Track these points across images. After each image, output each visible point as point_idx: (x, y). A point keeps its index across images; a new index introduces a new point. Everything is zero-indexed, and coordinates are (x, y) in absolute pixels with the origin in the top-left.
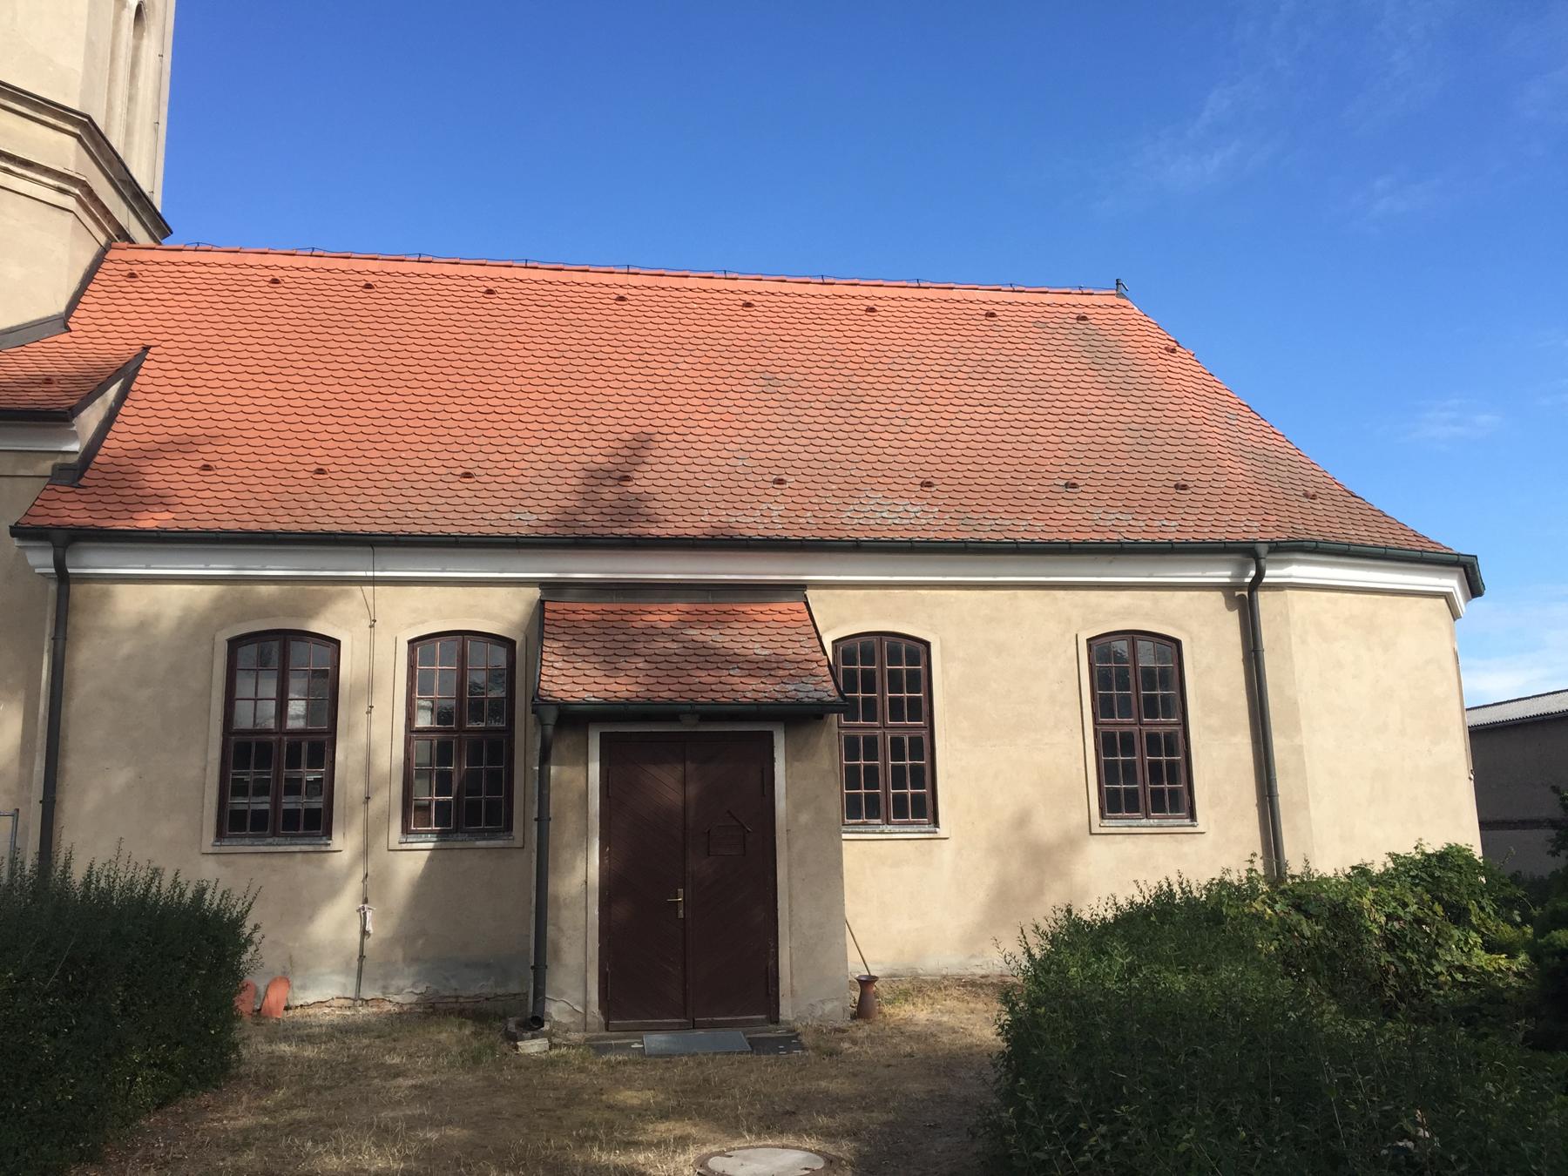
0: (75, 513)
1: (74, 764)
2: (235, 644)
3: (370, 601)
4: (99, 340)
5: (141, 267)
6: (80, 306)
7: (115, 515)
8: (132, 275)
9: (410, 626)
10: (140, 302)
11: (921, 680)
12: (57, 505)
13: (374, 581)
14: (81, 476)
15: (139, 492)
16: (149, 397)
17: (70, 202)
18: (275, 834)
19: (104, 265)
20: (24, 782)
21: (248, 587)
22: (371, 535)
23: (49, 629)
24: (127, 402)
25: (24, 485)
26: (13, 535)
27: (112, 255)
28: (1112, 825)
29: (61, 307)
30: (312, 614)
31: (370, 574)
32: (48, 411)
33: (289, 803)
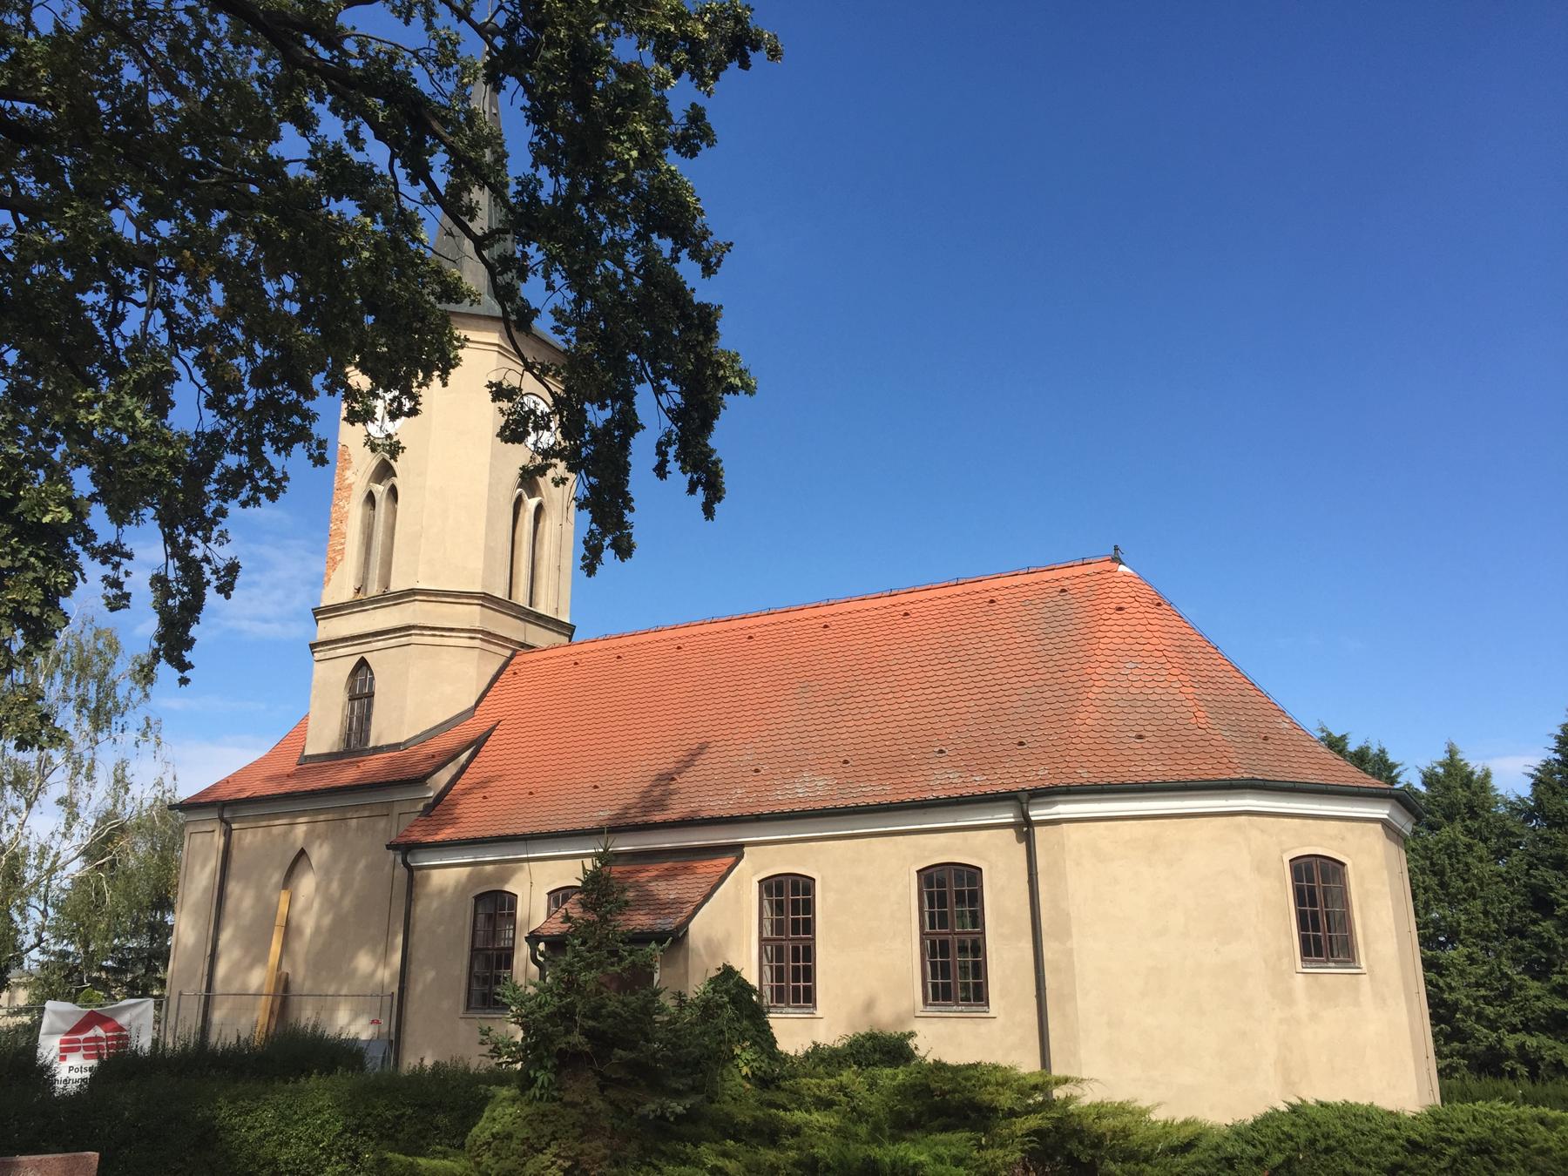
2: (478, 898)
11: (975, 898)
13: (528, 860)
17: (477, 643)
28: (931, 1011)
30: (505, 880)
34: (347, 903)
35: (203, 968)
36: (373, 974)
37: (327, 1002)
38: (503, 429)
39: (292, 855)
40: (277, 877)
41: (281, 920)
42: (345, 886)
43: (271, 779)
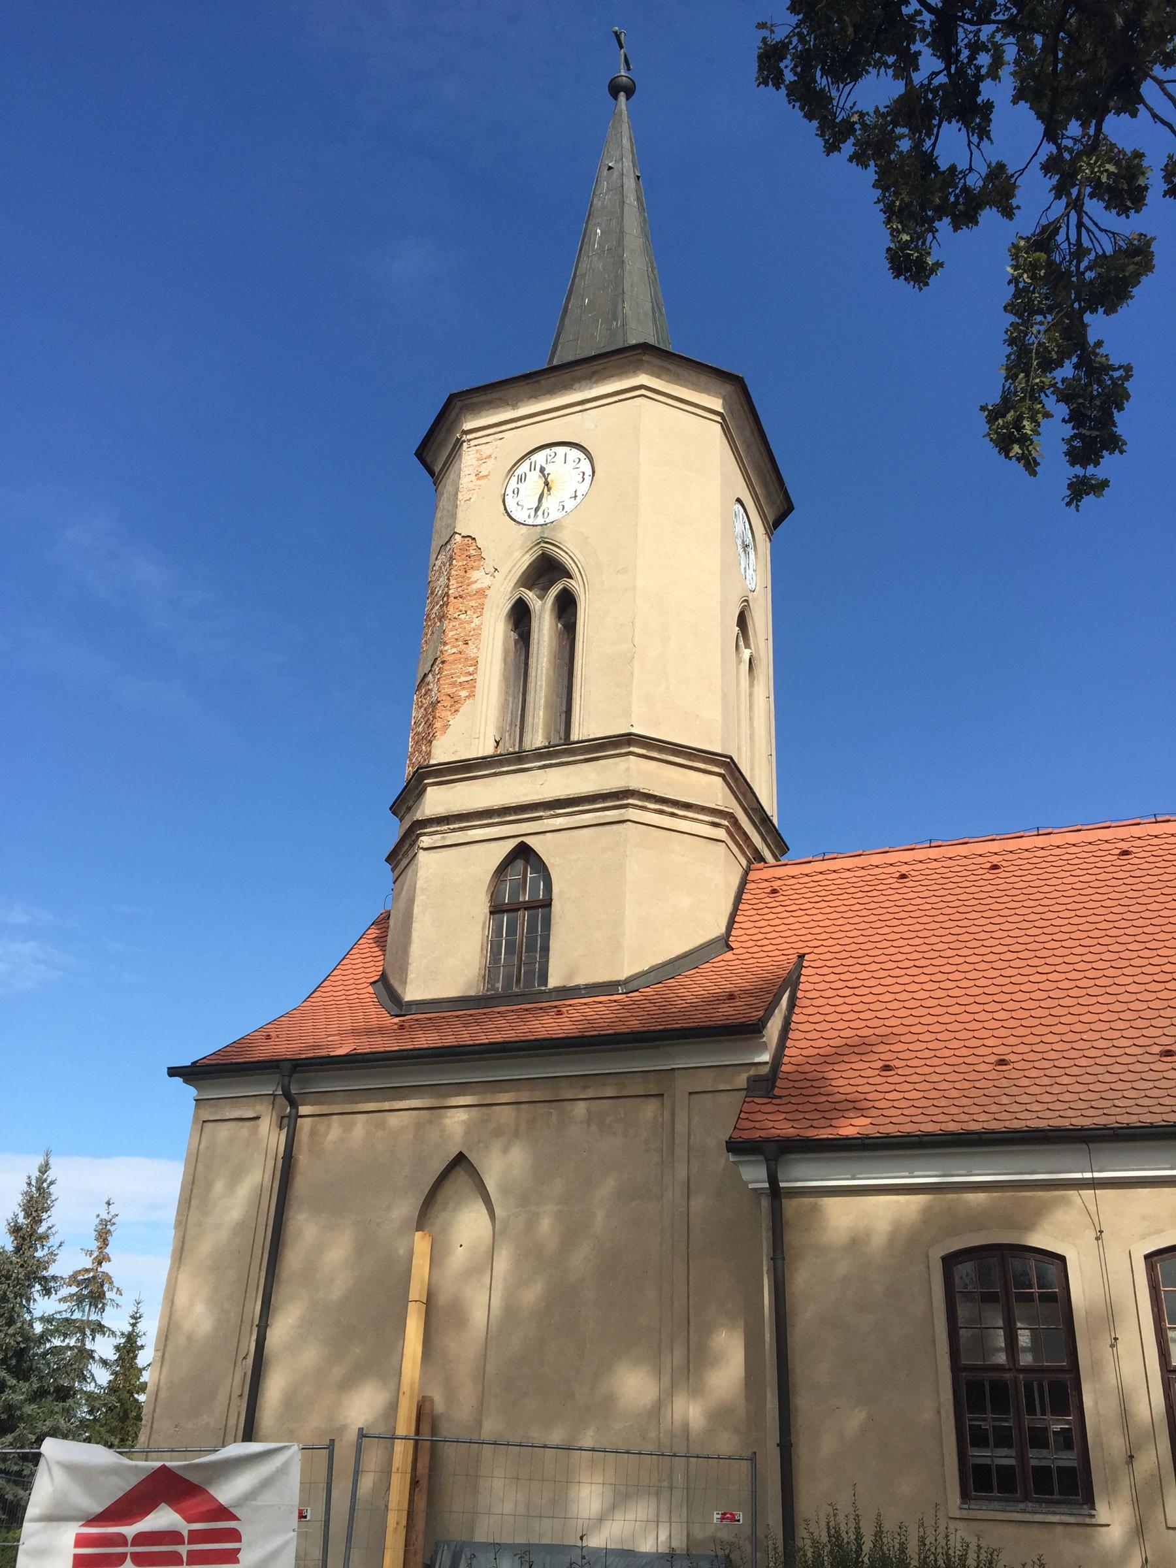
0: (779, 1125)
1: (803, 1401)
2: (950, 1261)
3: (1092, 1209)
4: (758, 956)
5: (780, 882)
6: (736, 926)
7: (815, 1123)
8: (774, 891)
9: (1144, 1237)
10: (786, 914)
12: (760, 1117)
14: (773, 1086)
15: (830, 1099)
16: (815, 1002)
17: (721, 834)
18: (1026, 1498)
19: (748, 886)
20: (755, 1416)
21: (954, 1196)
22: (1083, 1129)
23: (766, 1248)
24: (797, 1010)
25: (723, 1099)
26: (729, 1150)
27: (752, 876)
29: (721, 929)
30: (1029, 1225)
31: (1088, 1175)
32: (742, 1025)
33: (1037, 1458)
34: (581, 1259)
35: (236, 1380)
36: (657, 1410)
37: (546, 1465)
38: (1009, 305)
39: (437, 1166)
40: (405, 1207)
41: (417, 1291)
42: (571, 1232)
43: (355, 1032)
